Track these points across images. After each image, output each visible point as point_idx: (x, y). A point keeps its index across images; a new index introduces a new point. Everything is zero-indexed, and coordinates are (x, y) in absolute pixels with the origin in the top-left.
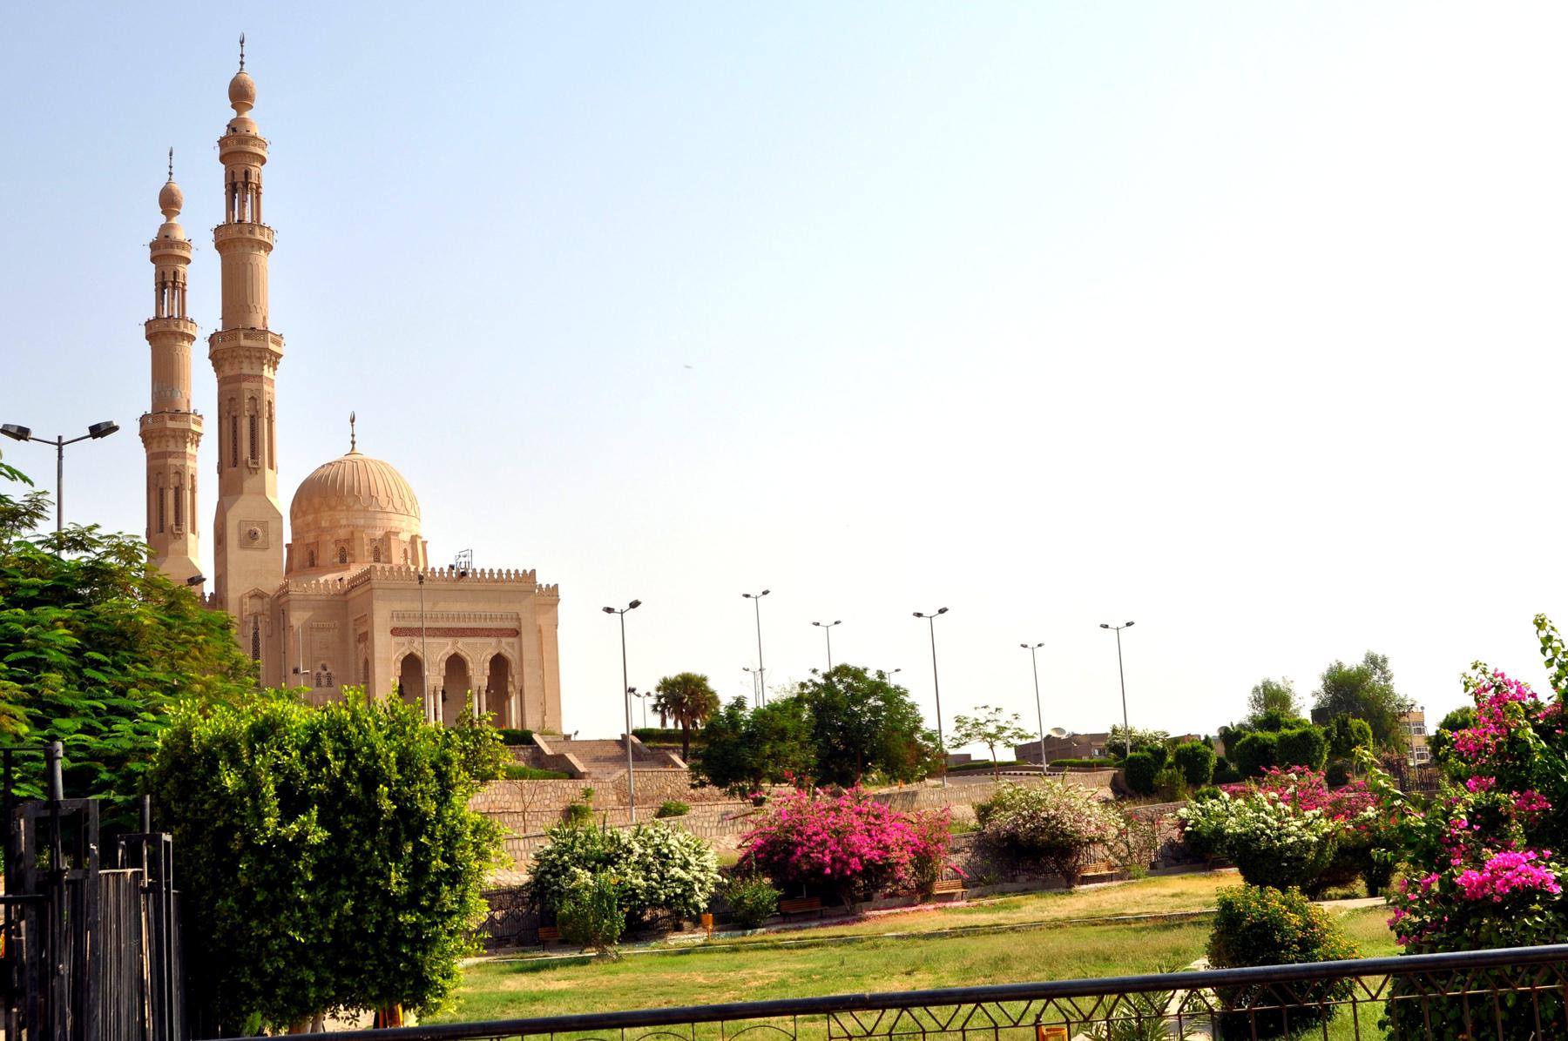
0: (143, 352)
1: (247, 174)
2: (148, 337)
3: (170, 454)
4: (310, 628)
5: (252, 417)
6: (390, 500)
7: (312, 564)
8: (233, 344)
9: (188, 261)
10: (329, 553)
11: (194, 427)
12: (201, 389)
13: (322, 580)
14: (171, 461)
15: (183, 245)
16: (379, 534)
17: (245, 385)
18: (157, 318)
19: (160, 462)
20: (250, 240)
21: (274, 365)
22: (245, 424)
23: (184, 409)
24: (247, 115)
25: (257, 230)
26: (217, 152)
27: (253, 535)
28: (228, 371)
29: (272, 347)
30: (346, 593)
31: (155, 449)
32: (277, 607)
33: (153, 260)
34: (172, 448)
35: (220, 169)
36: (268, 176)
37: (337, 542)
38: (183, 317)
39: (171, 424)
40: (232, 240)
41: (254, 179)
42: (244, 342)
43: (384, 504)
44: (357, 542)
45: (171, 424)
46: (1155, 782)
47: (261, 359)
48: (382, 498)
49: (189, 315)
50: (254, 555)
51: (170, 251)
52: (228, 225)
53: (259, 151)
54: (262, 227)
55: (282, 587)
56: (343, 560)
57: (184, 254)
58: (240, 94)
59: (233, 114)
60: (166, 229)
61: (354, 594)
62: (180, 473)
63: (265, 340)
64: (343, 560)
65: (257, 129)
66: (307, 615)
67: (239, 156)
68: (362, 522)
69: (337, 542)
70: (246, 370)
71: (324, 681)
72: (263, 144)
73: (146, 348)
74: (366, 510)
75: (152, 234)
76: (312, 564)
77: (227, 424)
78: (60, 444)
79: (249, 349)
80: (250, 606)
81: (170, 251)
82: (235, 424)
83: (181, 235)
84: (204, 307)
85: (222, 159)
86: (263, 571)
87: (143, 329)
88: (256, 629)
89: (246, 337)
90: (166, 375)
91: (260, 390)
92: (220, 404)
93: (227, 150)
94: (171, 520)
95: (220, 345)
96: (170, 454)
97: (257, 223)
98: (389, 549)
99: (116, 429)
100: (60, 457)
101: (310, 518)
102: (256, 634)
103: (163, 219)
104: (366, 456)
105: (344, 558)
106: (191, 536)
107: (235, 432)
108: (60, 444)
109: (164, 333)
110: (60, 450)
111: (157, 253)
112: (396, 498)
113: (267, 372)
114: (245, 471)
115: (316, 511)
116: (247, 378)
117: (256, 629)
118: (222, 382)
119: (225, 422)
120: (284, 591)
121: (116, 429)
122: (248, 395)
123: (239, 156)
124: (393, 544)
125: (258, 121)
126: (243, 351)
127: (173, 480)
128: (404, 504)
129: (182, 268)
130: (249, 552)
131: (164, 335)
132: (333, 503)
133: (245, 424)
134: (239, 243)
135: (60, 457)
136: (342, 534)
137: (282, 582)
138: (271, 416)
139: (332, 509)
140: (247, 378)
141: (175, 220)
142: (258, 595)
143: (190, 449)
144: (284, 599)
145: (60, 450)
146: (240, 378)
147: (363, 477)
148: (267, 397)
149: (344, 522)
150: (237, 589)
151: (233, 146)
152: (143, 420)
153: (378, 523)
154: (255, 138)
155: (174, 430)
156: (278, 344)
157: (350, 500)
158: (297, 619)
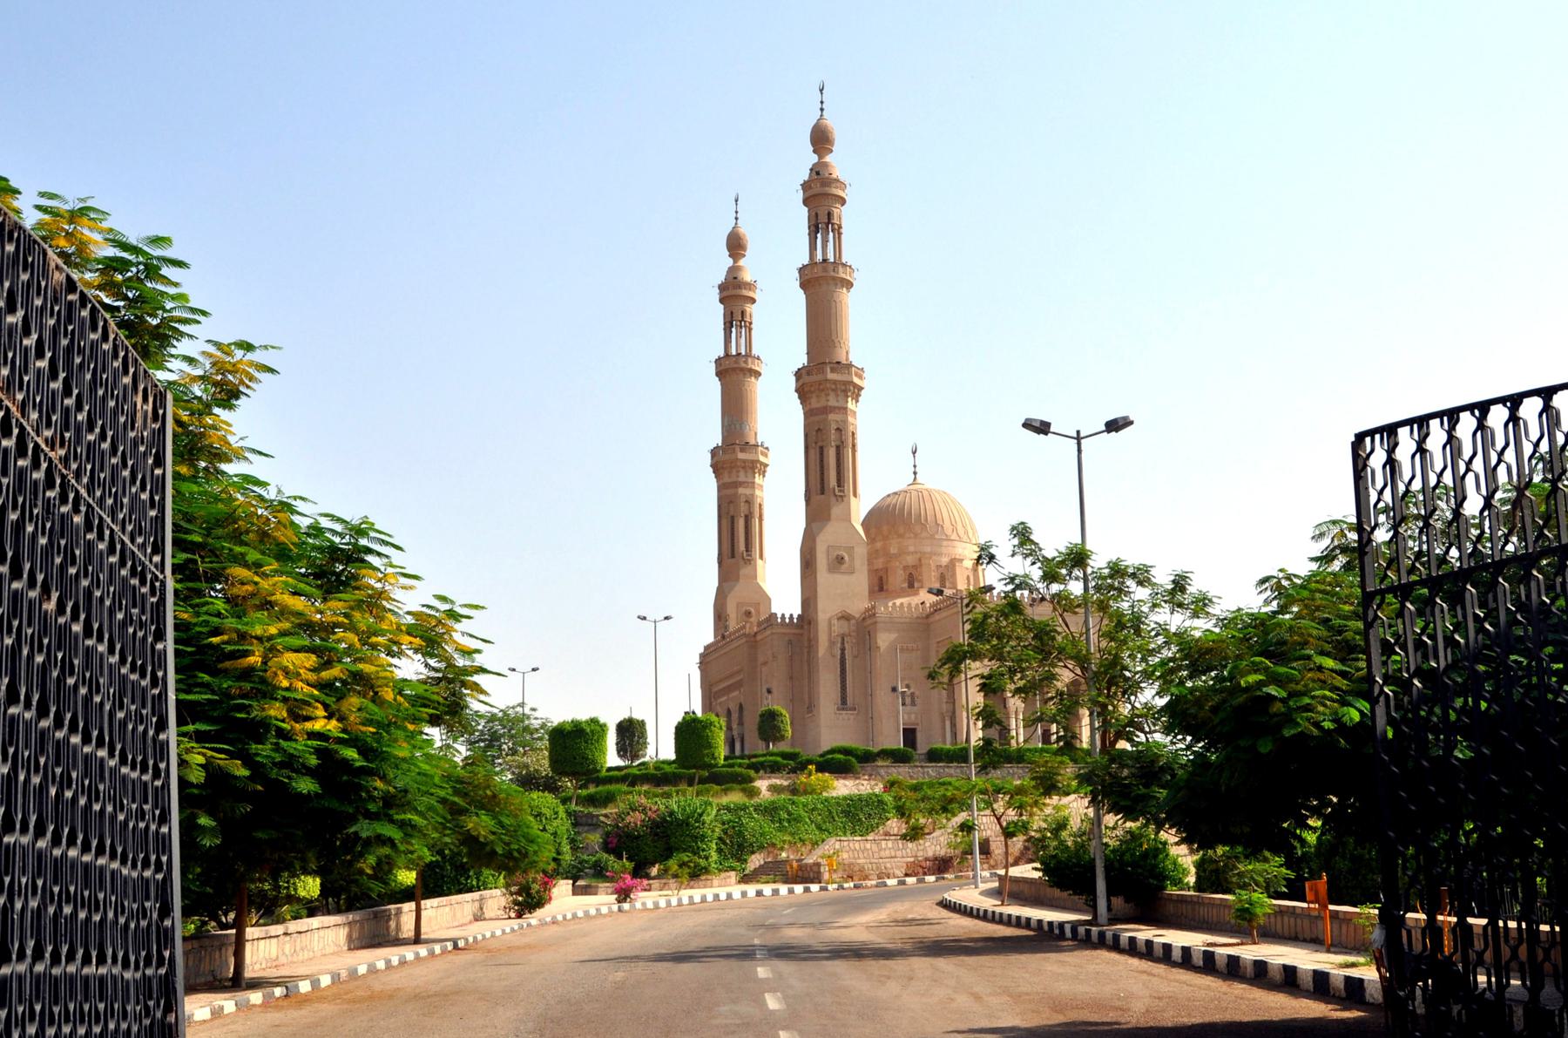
0: (715, 387)
1: (829, 215)
2: (717, 374)
3: (741, 484)
4: (893, 648)
5: (838, 447)
6: (955, 529)
7: (881, 589)
8: (820, 377)
9: (753, 301)
10: (897, 579)
11: (762, 459)
12: (779, 422)
13: (898, 602)
14: (741, 490)
15: (751, 286)
16: (945, 560)
17: (831, 417)
18: (727, 355)
19: (729, 492)
20: (834, 278)
21: (856, 398)
22: (831, 454)
23: (752, 442)
24: (828, 159)
25: (841, 269)
26: (800, 195)
27: (840, 560)
28: (815, 403)
29: (856, 380)
30: (928, 617)
31: (726, 479)
32: (863, 629)
33: (721, 301)
34: (742, 478)
35: (804, 212)
36: (848, 216)
37: (905, 568)
38: (749, 355)
39: (741, 456)
40: (817, 279)
41: (836, 221)
42: (831, 376)
43: (949, 532)
44: (924, 569)
45: (741, 456)
46: (486, 872)
47: (845, 391)
48: (947, 525)
49: (755, 352)
50: (840, 579)
51: (738, 292)
52: (813, 262)
53: (840, 193)
54: (844, 265)
55: (868, 610)
56: (911, 586)
57: (751, 294)
58: (821, 139)
59: (815, 159)
60: (733, 272)
61: (937, 617)
62: (749, 502)
63: (850, 373)
64: (911, 586)
65: (838, 172)
66: (893, 636)
67: (821, 200)
68: (928, 549)
69: (905, 568)
70: (832, 402)
71: (908, 700)
72: (843, 186)
73: (716, 385)
74: (932, 537)
75: (721, 278)
76: (881, 589)
77: (814, 454)
78: (1078, 438)
79: (835, 382)
80: (839, 628)
81: (738, 292)
82: (822, 454)
83: (747, 277)
84: (780, 340)
85: (806, 202)
86: (847, 593)
87: (713, 366)
88: (843, 650)
89: (833, 370)
90: (735, 409)
91: (845, 422)
92: (806, 436)
93: (810, 193)
94: (742, 546)
95: (806, 379)
96: (741, 484)
97: (838, 263)
98: (954, 575)
99: (1131, 423)
100: (1079, 451)
101: (879, 545)
102: (843, 654)
103: (730, 262)
104: (928, 486)
105: (912, 584)
106: (759, 562)
107: (822, 461)
108: (1078, 438)
109: (734, 369)
110: (1079, 444)
111: (726, 293)
112: (960, 527)
113: (851, 405)
114: (833, 499)
115: (885, 538)
116: (833, 409)
117: (843, 650)
118: (809, 414)
119: (812, 452)
120: (870, 614)
121: (1131, 423)
122: (834, 426)
123: (821, 200)
124: (958, 570)
125: (838, 163)
126: (825, 385)
127: (743, 508)
128: (966, 533)
129: (749, 308)
130: (838, 577)
131: (734, 372)
132: (901, 531)
133: (831, 454)
134: (822, 283)
135: (1079, 451)
136: (910, 560)
137: (867, 605)
138: (854, 446)
139: (901, 536)
140: (833, 409)
141: (741, 262)
142: (845, 617)
143: (758, 479)
144: (869, 622)
145: (1079, 444)
146: (826, 410)
147: (929, 506)
148: (851, 428)
149: (911, 549)
150: (826, 611)
151: (817, 189)
152: (714, 452)
153: (944, 550)
154: (837, 180)
155: (744, 461)
156: (860, 377)
157: (918, 529)
158: (884, 640)
